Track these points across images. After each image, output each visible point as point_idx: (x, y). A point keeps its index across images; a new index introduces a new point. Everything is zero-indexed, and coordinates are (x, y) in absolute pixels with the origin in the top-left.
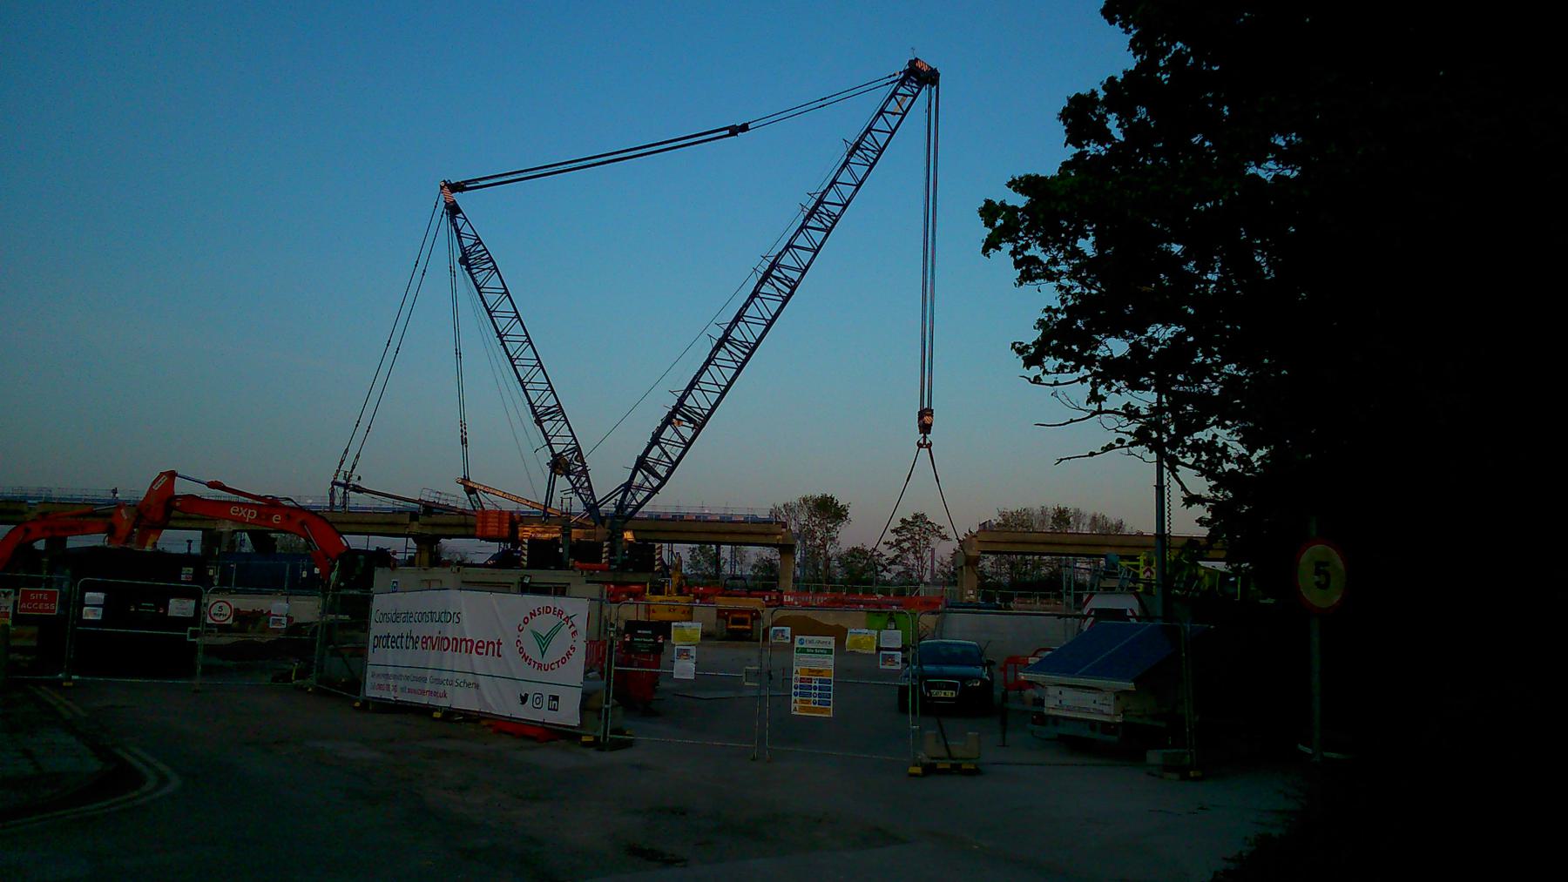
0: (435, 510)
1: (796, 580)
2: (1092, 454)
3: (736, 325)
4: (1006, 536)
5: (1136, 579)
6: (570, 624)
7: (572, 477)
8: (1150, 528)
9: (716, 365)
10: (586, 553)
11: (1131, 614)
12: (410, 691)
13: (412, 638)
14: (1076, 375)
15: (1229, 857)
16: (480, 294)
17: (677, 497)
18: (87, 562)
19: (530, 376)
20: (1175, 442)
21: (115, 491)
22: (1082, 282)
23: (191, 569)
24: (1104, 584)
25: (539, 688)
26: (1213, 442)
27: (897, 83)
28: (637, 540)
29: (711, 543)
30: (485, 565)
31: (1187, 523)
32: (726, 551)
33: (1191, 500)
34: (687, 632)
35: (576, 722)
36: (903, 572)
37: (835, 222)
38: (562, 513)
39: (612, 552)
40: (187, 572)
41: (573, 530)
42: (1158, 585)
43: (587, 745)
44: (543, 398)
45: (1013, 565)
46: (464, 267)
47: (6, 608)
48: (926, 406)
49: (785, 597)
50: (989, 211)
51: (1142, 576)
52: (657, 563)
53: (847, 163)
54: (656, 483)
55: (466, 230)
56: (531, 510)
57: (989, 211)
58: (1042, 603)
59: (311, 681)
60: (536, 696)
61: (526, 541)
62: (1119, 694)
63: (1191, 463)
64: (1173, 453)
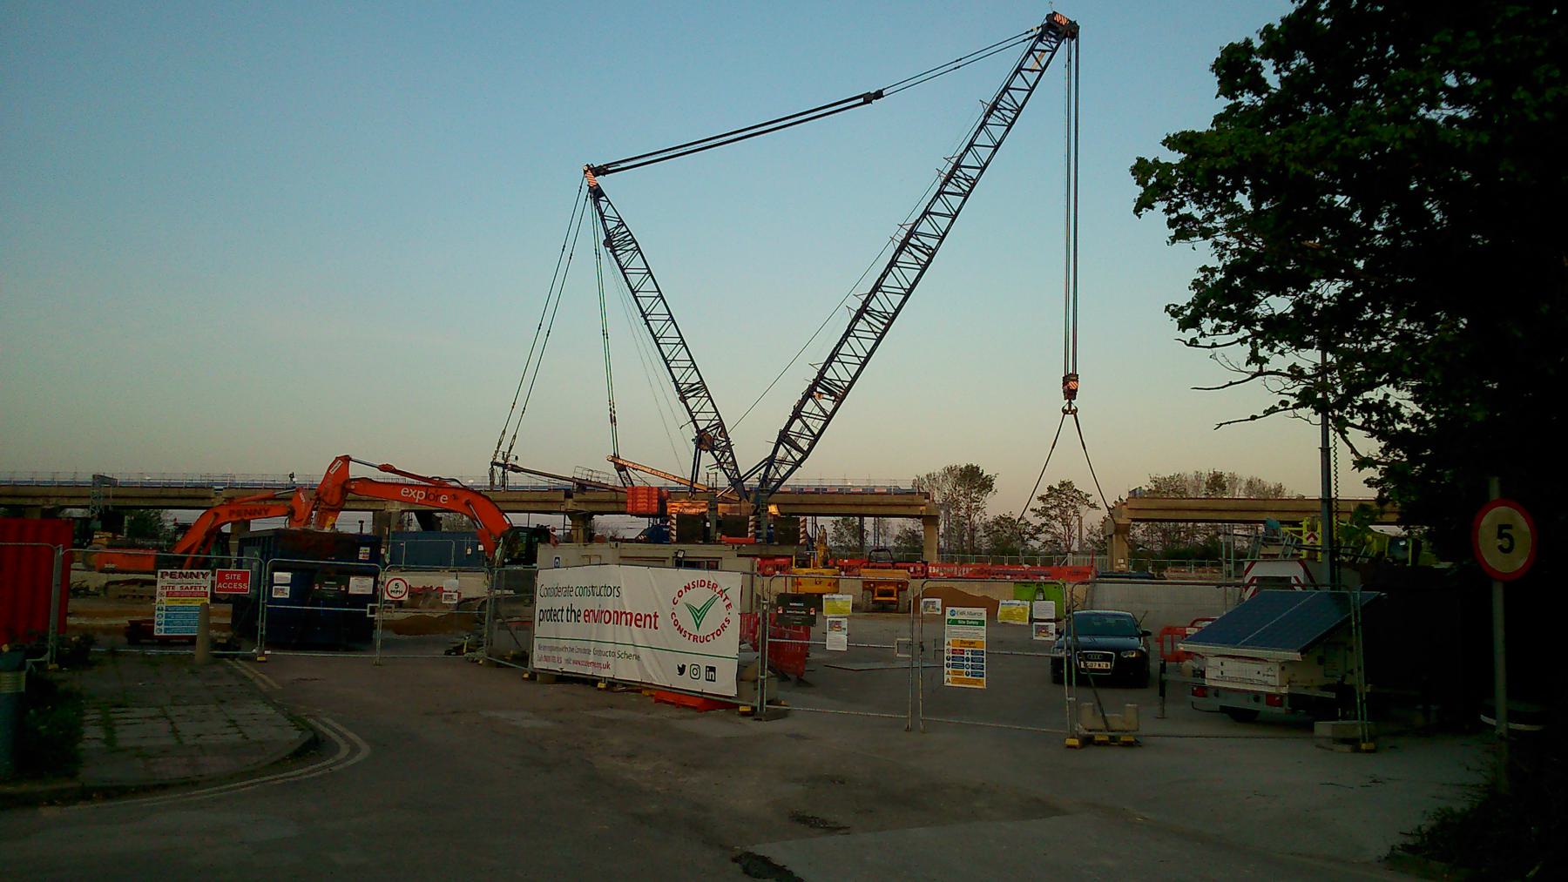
0: (588, 488)
1: (940, 551)
2: (1254, 418)
3: (874, 295)
4: (1160, 503)
5: (1300, 547)
6: (724, 597)
7: (717, 453)
8: (1314, 491)
9: (855, 336)
10: (732, 528)
11: (1296, 582)
12: (575, 662)
13: (574, 611)
14: (1235, 336)
15: (1408, 831)
16: (624, 274)
17: (814, 473)
18: (273, 545)
19: (674, 354)
20: (1341, 404)
21: (292, 476)
22: (1239, 236)
23: (368, 549)
24: (1265, 551)
25: (695, 660)
26: (1384, 402)
27: (1034, 39)
28: (782, 514)
29: (854, 515)
30: (637, 540)
31: (1354, 486)
32: (869, 523)
33: (1362, 463)
34: (839, 603)
35: (733, 693)
36: (1050, 541)
37: (973, 185)
38: (710, 489)
39: (758, 526)
40: (364, 552)
41: (719, 505)
42: (1324, 552)
43: (745, 714)
44: (686, 375)
45: (1165, 533)
46: (608, 249)
47: (205, 588)
48: (1070, 371)
49: (930, 568)
50: (1141, 169)
51: (1305, 542)
52: (801, 536)
53: (984, 124)
54: (798, 456)
55: (609, 212)
56: (678, 485)
57: (1141, 169)
58: (1197, 572)
59: (480, 654)
60: (693, 667)
61: (675, 516)
62: (1284, 665)
63: (1360, 424)
64: (1341, 414)
